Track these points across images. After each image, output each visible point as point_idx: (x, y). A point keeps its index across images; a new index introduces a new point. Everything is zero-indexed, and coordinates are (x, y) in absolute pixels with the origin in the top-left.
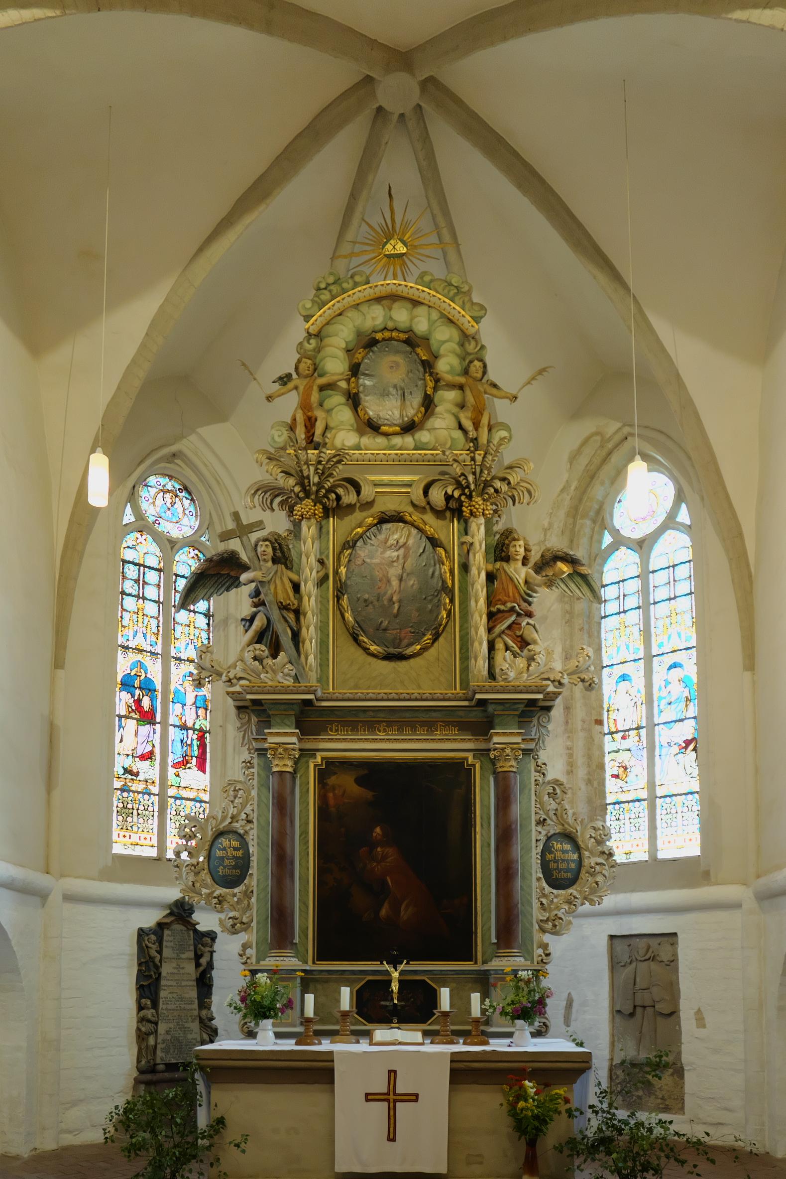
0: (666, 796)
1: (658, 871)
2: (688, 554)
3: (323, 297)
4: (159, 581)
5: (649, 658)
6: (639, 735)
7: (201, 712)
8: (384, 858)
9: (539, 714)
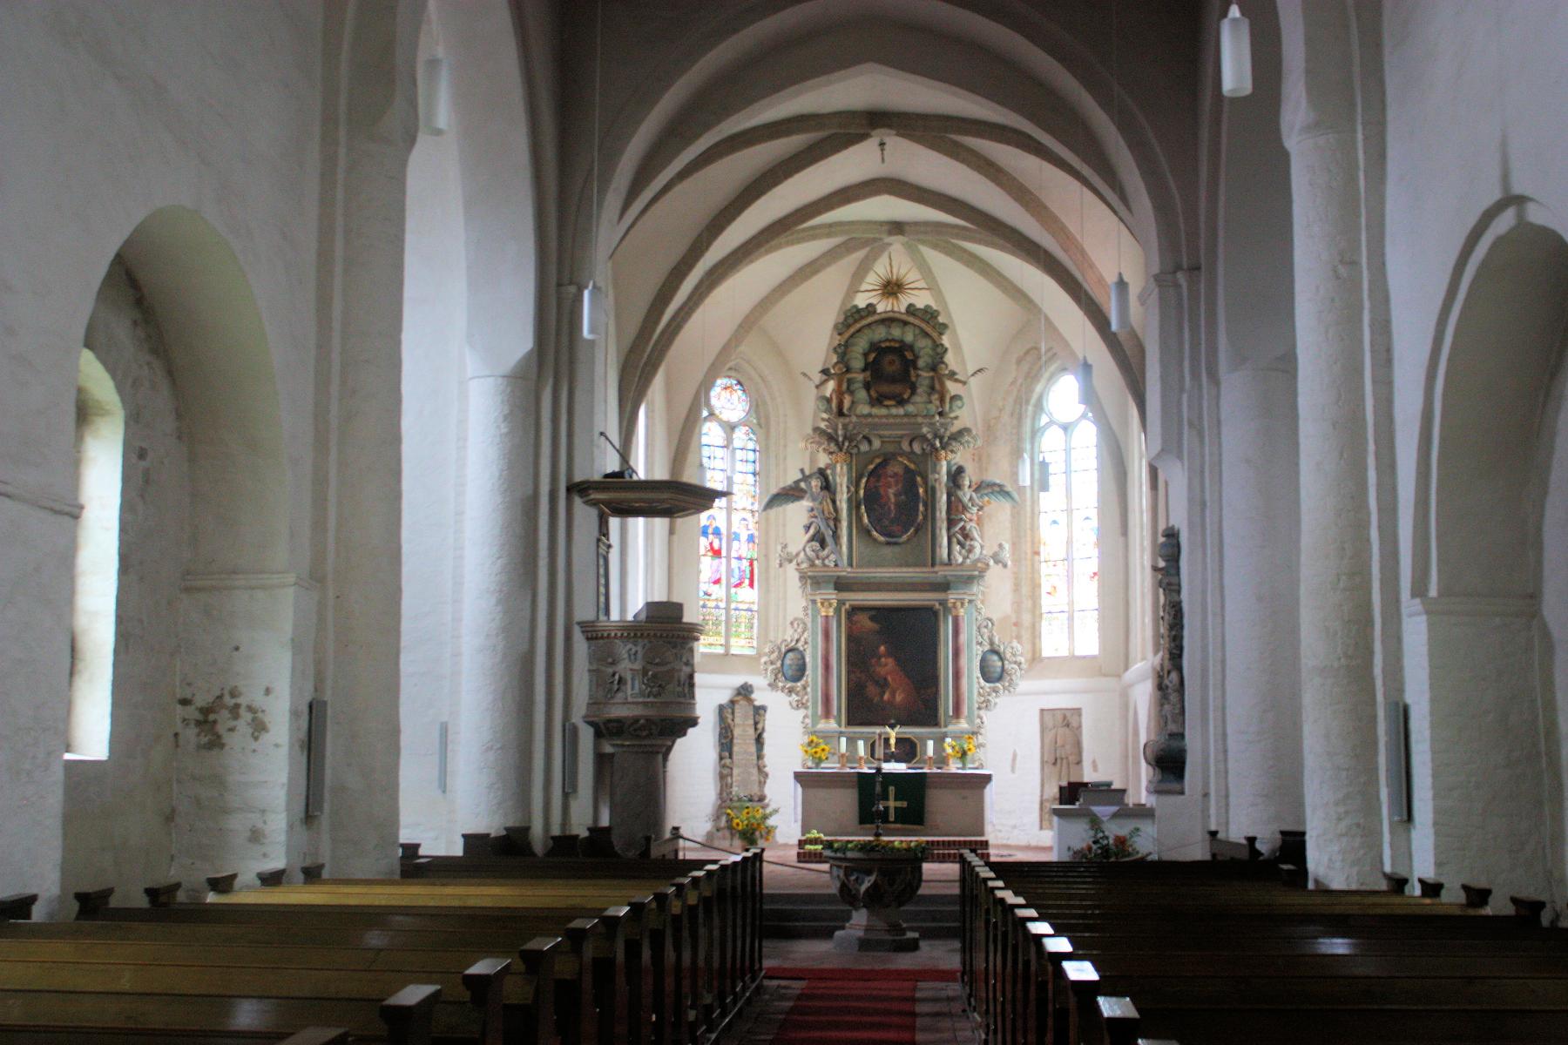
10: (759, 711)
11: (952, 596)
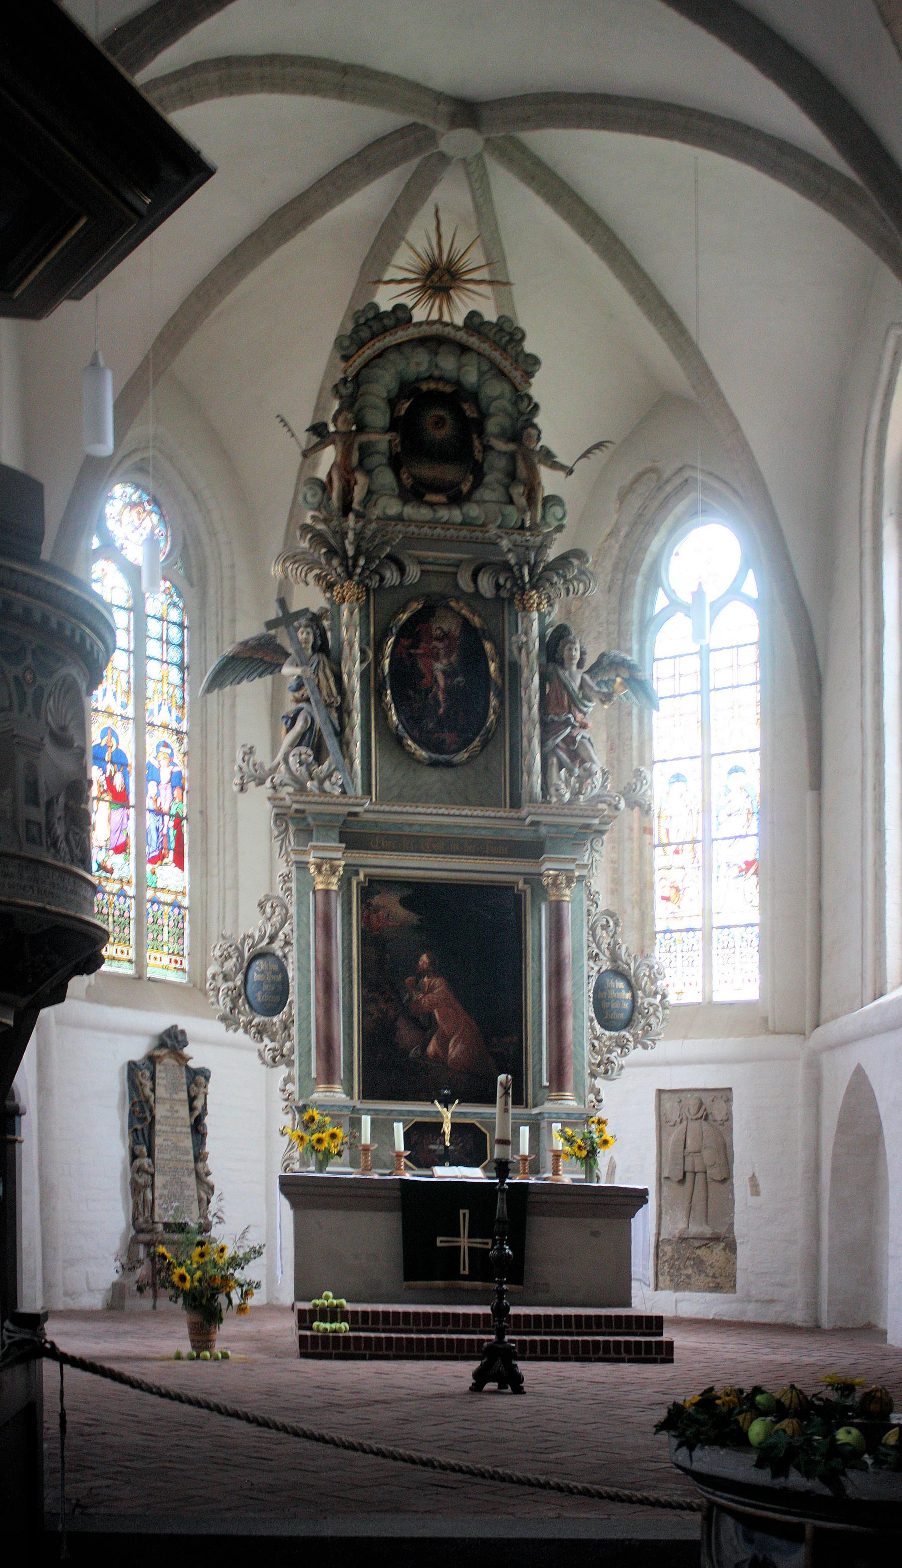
0: (723, 927)
1: (708, 1015)
5: (706, 758)
6: (693, 849)
7: (177, 792)
8: (431, 989)
9: (592, 837)
10: (197, 1078)
11: (549, 867)
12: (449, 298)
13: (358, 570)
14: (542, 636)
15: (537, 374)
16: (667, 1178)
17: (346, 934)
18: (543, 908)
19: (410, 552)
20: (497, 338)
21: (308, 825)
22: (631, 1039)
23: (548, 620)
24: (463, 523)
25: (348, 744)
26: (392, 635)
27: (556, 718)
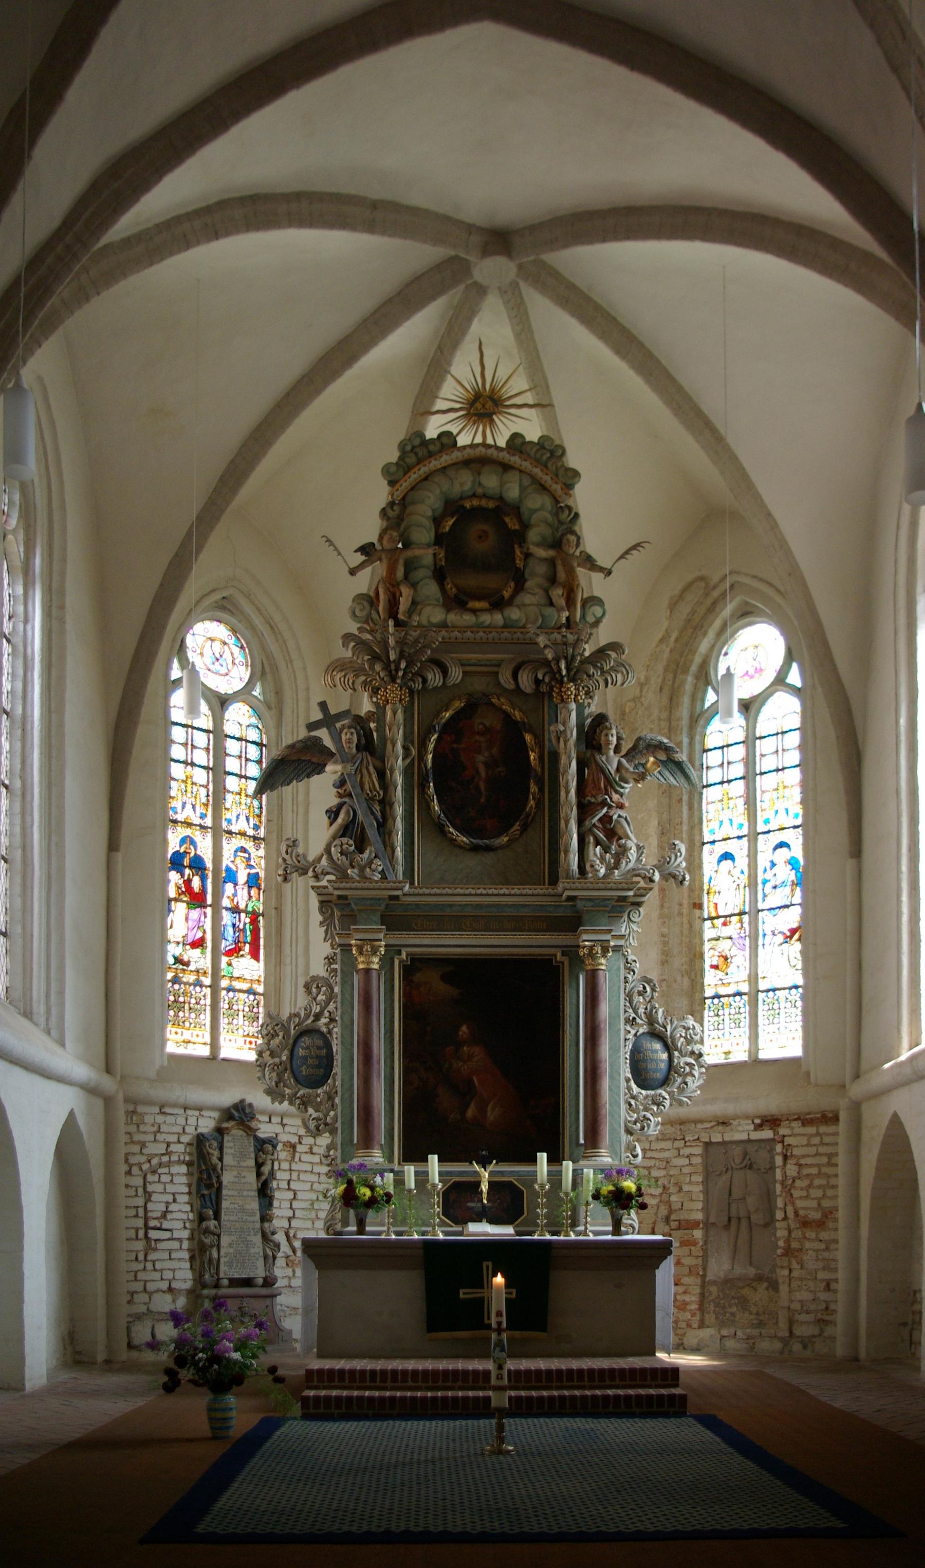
2: (796, 722)
3: (408, 460)
4: (209, 744)
5: (753, 836)
6: (741, 922)
7: (254, 892)
11: (586, 939)
12: (492, 422)
13: (401, 673)
14: (580, 726)
15: (577, 487)
16: (713, 1224)
17: (388, 1009)
18: (581, 977)
19: (453, 655)
20: (538, 456)
21: (353, 910)
22: (667, 1097)
23: (587, 711)
24: (505, 626)
25: (390, 833)
26: (435, 731)
27: (593, 800)
